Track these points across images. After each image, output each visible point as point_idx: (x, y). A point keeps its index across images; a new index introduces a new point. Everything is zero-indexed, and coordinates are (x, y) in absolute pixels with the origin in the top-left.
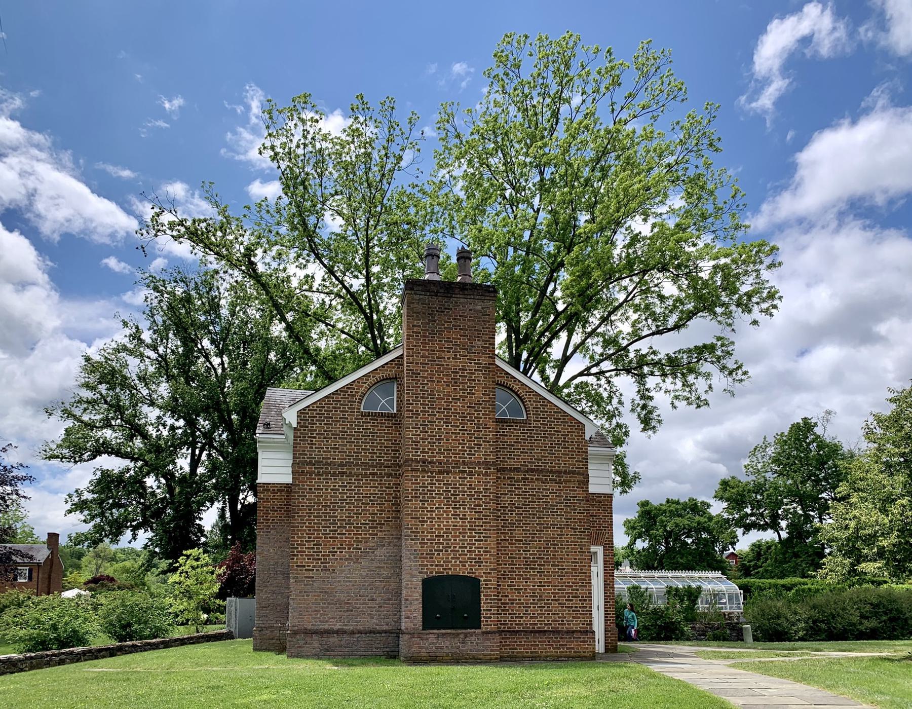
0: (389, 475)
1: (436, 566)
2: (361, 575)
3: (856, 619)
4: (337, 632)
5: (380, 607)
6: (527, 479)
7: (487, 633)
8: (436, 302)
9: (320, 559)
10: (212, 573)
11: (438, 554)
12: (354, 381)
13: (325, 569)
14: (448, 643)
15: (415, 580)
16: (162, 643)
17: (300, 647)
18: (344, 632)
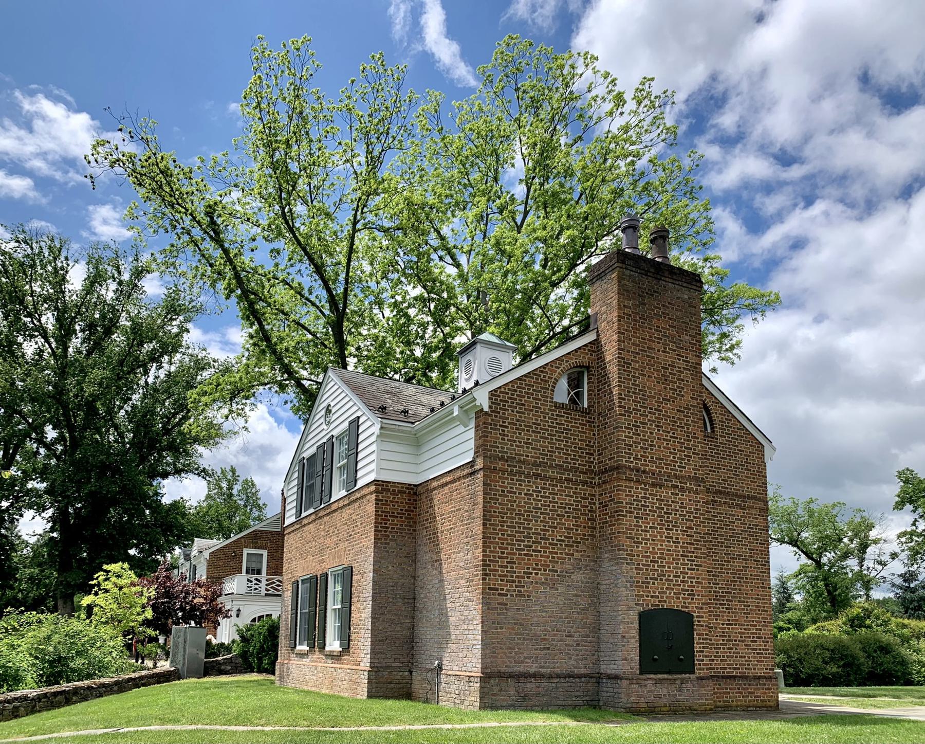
0: (585, 483)
1: (652, 597)
2: (558, 604)
3: (819, 663)
4: (534, 676)
5: (578, 645)
6: (716, 501)
7: (702, 678)
8: (647, 282)
9: (514, 581)
10: (141, 594)
11: (654, 583)
12: (547, 364)
13: (520, 594)
14: (665, 691)
15: (632, 613)
16: (116, 683)
17: (494, 695)
18: (542, 676)
